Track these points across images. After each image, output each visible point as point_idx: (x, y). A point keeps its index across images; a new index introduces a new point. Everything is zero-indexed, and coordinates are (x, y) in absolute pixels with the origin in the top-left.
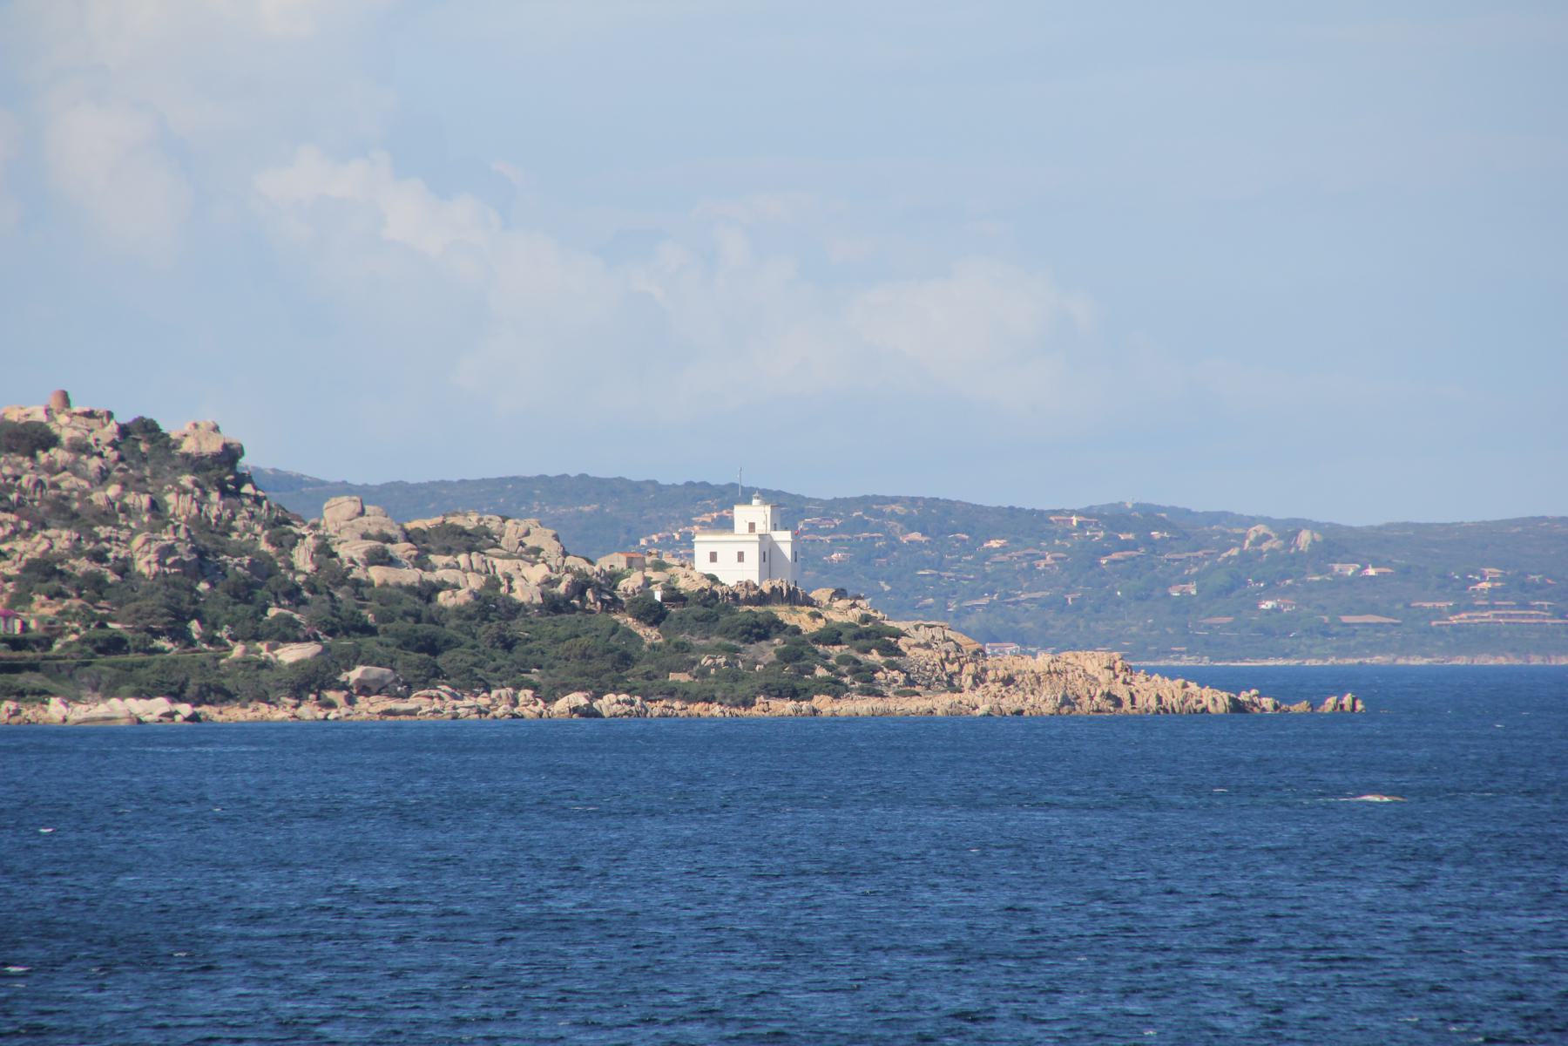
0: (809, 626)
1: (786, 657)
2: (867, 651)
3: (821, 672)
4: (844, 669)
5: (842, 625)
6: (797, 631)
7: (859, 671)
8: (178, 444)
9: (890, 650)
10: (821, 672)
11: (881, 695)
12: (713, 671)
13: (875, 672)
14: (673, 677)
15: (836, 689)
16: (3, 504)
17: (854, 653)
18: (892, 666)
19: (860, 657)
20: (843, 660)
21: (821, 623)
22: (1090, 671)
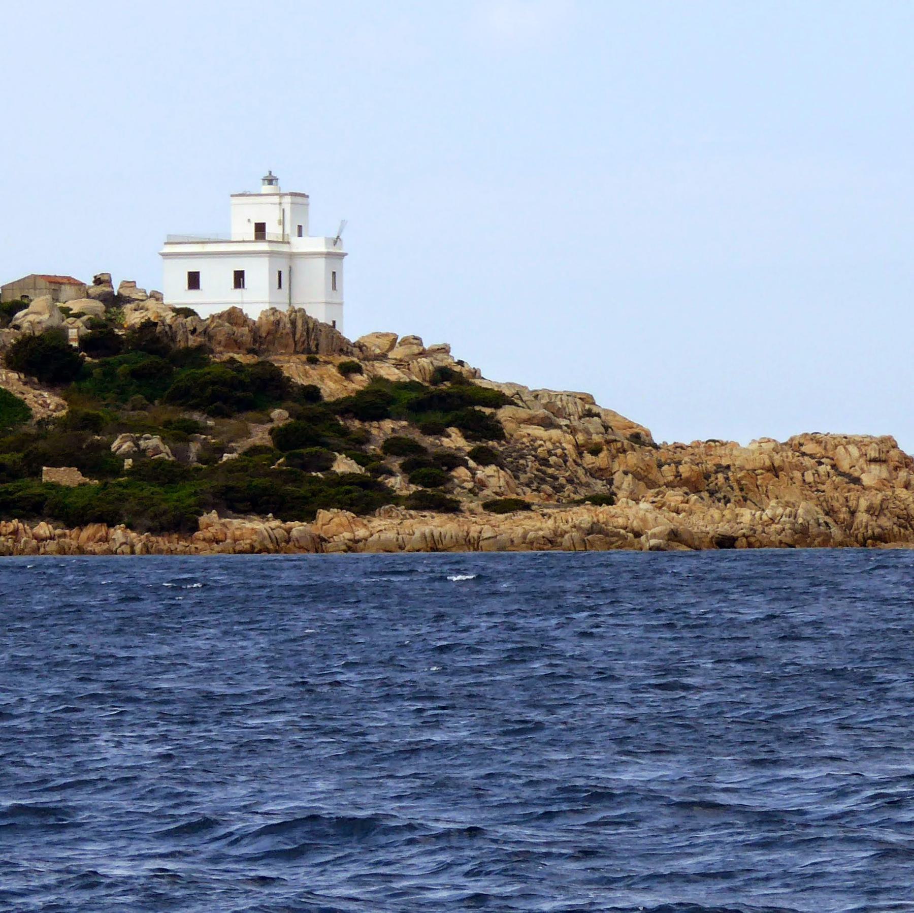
0: (332, 386)
1: (284, 439)
2: (439, 431)
3: (343, 465)
4: (395, 463)
5: (401, 386)
6: (312, 393)
7: (419, 464)
8: (59, 334)
9: (483, 429)
10: (343, 465)
11: (452, 508)
12: (128, 463)
13: (452, 467)
14: (52, 475)
15: (365, 497)
16: (913, 550)
17: (416, 435)
18: (483, 457)
19: (427, 441)
20: (393, 446)
21: (360, 382)
22: (845, 466)
